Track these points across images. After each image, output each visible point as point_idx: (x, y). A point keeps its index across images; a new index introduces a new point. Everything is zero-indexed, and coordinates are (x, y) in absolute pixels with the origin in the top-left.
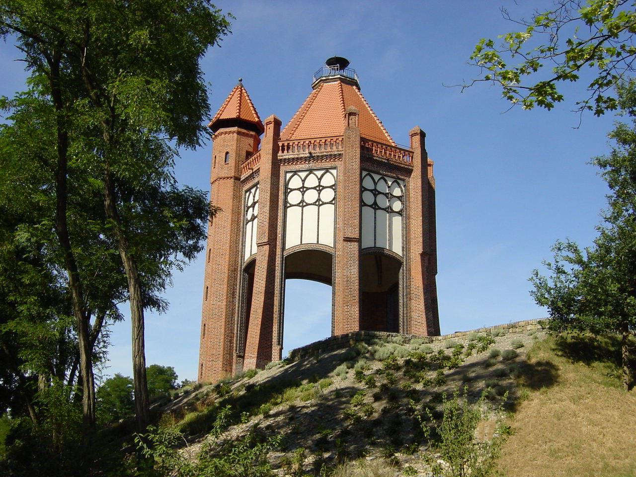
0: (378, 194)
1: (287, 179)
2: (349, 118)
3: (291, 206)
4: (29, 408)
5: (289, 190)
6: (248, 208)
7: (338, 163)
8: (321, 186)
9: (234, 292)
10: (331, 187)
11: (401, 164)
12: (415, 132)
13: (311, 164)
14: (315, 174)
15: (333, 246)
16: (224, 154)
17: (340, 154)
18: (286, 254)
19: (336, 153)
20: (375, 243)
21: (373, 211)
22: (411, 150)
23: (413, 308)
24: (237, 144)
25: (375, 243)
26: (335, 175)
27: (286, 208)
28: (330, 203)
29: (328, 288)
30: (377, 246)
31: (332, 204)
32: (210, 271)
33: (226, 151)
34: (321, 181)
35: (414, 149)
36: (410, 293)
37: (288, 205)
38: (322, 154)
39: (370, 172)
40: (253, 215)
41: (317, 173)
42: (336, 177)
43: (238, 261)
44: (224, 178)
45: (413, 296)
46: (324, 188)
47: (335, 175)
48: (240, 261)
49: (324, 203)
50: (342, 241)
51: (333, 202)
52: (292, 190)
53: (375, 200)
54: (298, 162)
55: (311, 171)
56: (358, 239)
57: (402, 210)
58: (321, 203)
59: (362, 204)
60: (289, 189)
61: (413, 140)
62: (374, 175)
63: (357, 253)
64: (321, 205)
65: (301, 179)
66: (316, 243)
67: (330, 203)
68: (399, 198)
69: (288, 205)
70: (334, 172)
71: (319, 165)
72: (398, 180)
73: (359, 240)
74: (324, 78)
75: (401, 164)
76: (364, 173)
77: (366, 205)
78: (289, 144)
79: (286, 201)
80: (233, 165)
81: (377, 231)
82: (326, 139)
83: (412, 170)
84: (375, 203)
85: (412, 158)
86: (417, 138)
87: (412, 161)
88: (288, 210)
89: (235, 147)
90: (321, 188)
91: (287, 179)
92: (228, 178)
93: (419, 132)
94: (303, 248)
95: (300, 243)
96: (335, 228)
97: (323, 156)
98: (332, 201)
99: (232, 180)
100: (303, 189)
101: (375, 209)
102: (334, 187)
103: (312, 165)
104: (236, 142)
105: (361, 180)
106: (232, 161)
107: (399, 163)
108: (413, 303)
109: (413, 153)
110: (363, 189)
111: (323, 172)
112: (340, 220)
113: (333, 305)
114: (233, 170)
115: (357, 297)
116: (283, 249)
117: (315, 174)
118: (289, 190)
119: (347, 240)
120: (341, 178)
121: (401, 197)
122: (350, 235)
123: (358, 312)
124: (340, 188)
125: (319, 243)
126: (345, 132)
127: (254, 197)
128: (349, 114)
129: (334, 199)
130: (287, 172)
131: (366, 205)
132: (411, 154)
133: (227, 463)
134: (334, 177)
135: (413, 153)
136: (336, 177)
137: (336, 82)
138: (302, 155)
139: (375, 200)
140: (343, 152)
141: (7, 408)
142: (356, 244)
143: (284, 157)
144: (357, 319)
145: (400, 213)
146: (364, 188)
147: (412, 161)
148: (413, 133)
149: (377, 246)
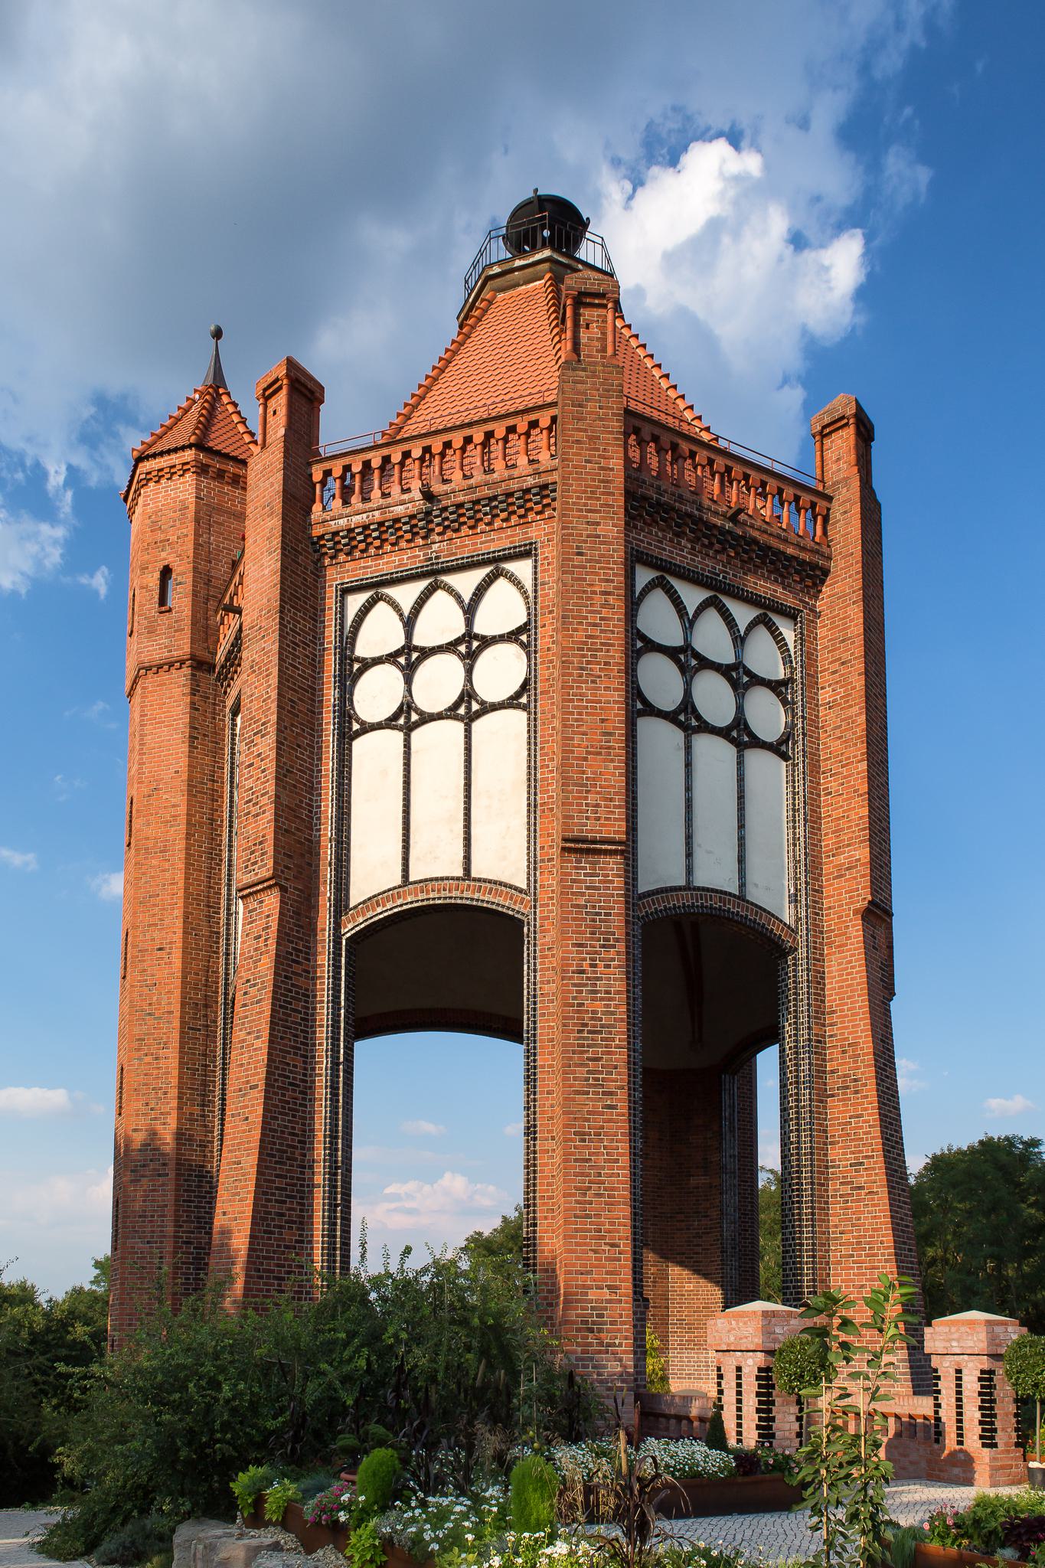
0: (697, 670)
2: (576, 316)
3: (367, 728)
4: (240, 1243)
5: (356, 666)
7: (539, 531)
9: (205, 1084)
10: (512, 637)
11: (785, 541)
12: (836, 416)
13: (435, 547)
14: (450, 590)
16: (157, 575)
17: (545, 487)
18: (348, 929)
19: (530, 481)
20: (689, 871)
21: (678, 735)
22: (820, 489)
23: (834, 1131)
24: (197, 535)
25: (689, 871)
26: (528, 584)
27: (346, 737)
28: (511, 703)
29: (508, 1054)
30: (701, 879)
31: (519, 706)
32: (126, 1009)
33: (160, 566)
35: (834, 484)
36: (822, 1072)
37: (356, 726)
38: (474, 497)
39: (666, 573)
41: (457, 581)
42: (531, 594)
43: (217, 972)
44: (160, 667)
45: (833, 1083)
46: (487, 642)
47: (528, 584)
48: (222, 970)
49: (488, 708)
50: (555, 852)
51: (524, 700)
52: (368, 664)
54: (384, 541)
55: (434, 575)
56: (620, 843)
57: (787, 737)
58: (475, 707)
59: (639, 706)
60: (358, 660)
61: (828, 454)
63: (618, 908)
64: (479, 715)
65: (401, 615)
66: (460, 873)
67: (511, 703)
68: (777, 687)
69: (356, 726)
70: (522, 569)
71: (467, 544)
72: (771, 615)
73: (628, 849)
74: (496, 270)
75: (785, 541)
76: (644, 576)
77: (650, 710)
78: (347, 468)
79: (345, 712)
80: (187, 612)
81: (698, 838)
82: (489, 427)
83: (826, 572)
84: (688, 704)
85: (826, 520)
86: (844, 442)
87: (825, 533)
88: (358, 745)
89: (189, 547)
92: (171, 665)
93: (851, 410)
94: (410, 900)
95: (398, 881)
96: (532, 807)
97: (477, 502)
99: (186, 670)
100: (409, 655)
102: (524, 638)
103: (440, 548)
104: (191, 526)
105: (633, 604)
106: (181, 598)
107: (778, 537)
108: (836, 1110)
109: (830, 499)
110: (639, 645)
111: (480, 574)
112: (550, 775)
113: (530, 1131)
114: (188, 631)
115: (622, 1095)
116: (341, 905)
117: (450, 590)
118: (356, 666)
119: (578, 847)
120: (551, 592)
121: (784, 683)
122: (591, 828)
123: (625, 1161)
124: (546, 636)
125: (474, 874)
126: (561, 390)
128: (574, 298)
129: (525, 687)
130: (346, 591)
131: (650, 710)
132: (821, 504)
134: (524, 593)
135: (830, 499)
136: (531, 594)
137: (538, 283)
138: (399, 510)
140: (556, 477)
142: (613, 865)
143: (333, 526)
144: (623, 1192)
145: (779, 749)
146: (643, 638)
147: (825, 533)
148: (827, 420)
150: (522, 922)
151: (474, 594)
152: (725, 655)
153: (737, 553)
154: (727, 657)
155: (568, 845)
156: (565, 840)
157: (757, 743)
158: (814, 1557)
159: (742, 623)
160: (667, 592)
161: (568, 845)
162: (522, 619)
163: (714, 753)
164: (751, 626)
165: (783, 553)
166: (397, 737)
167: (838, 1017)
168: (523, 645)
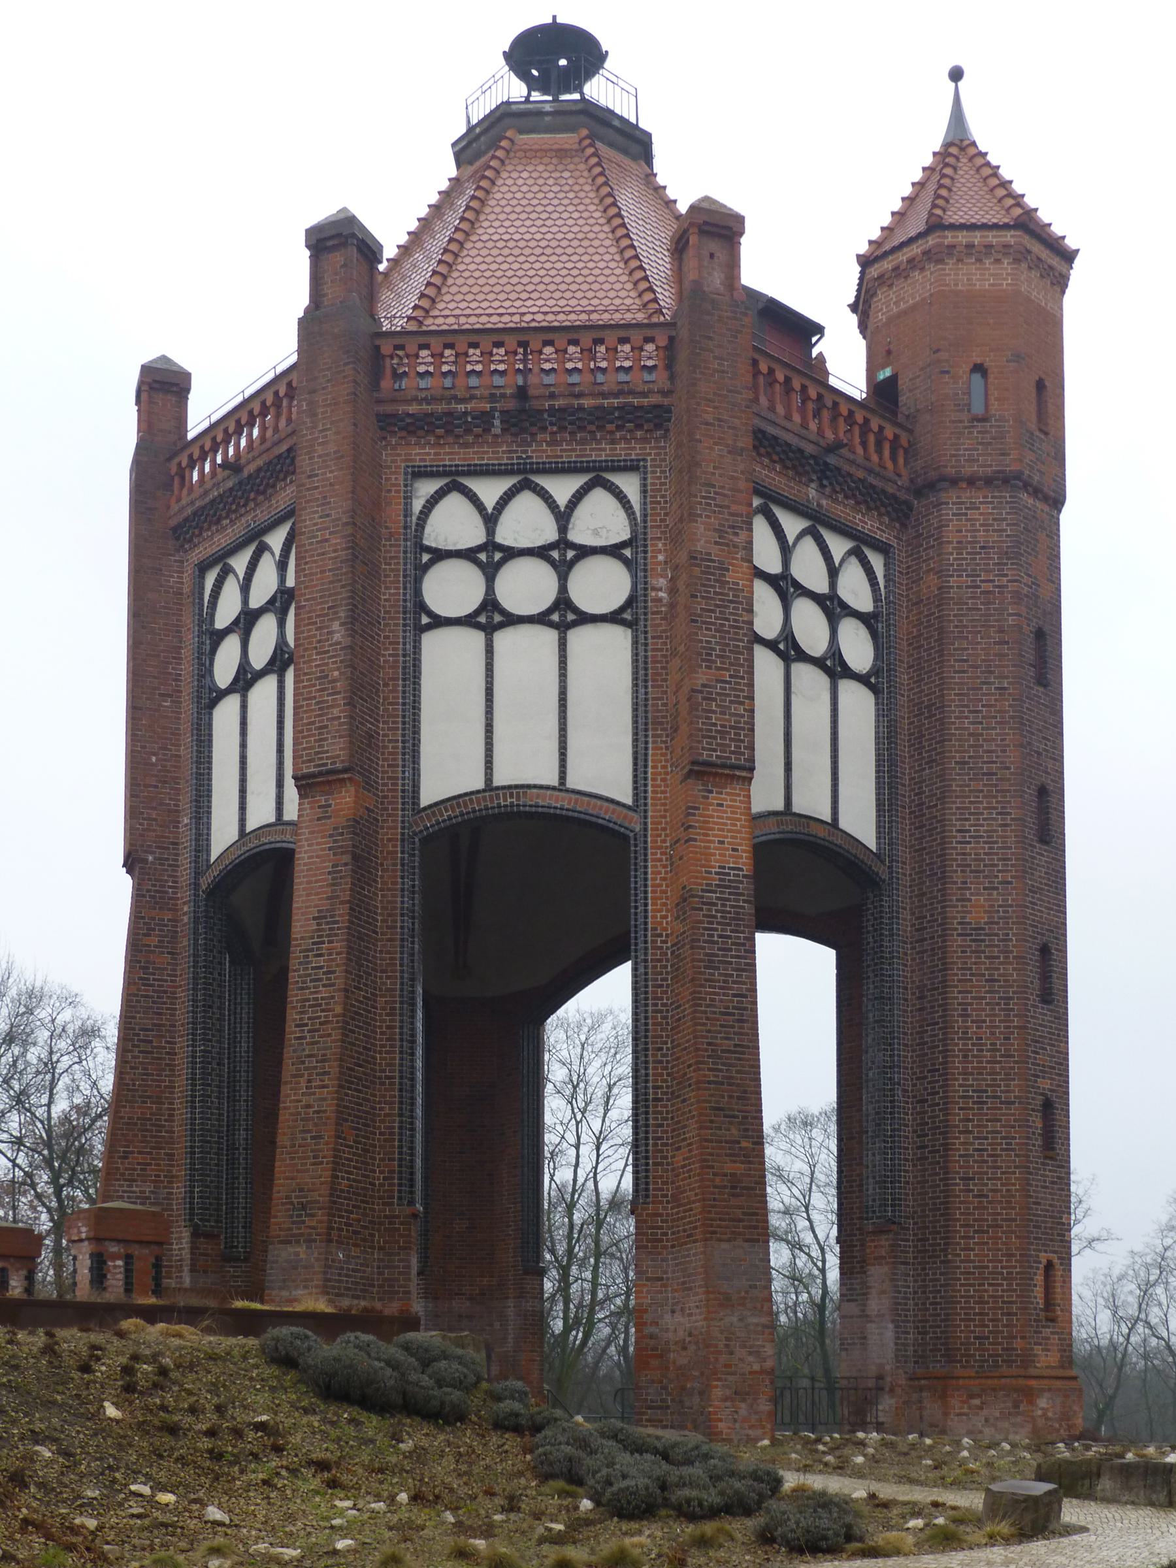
1: (418, 505)
6: (219, 636)
8: (573, 546)
15: (629, 801)
30: (499, 780)
34: (568, 521)
40: (244, 665)
42: (637, 507)
51: (627, 616)
53: (563, 588)
62: (548, 483)
66: (554, 781)
70: (629, 485)
90: (498, 556)
91: (418, 505)
98: (622, 609)
101: (563, 628)
102: (627, 552)
127: (245, 588)
129: (630, 602)
133: (634, 1509)
136: (637, 507)
139: (563, 588)
141: (578, 1414)
149: (570, 784)
150: (628, 837)
151: (570, 501)
152: (820, 585)
153: (842, 490)
154: (822, 587)
155: (696, 768)
156: (693, 763)
157: (803, 657)
158: (767, 1508)
159: (791, 534)
160: (860, 561)
161: (696, 768)
162: (625, 535)
163: (809, 679)
164: (799, 537)
165: (884, 492)
166: (476, 639)
167: (986, 946)
168: (626, 562)
